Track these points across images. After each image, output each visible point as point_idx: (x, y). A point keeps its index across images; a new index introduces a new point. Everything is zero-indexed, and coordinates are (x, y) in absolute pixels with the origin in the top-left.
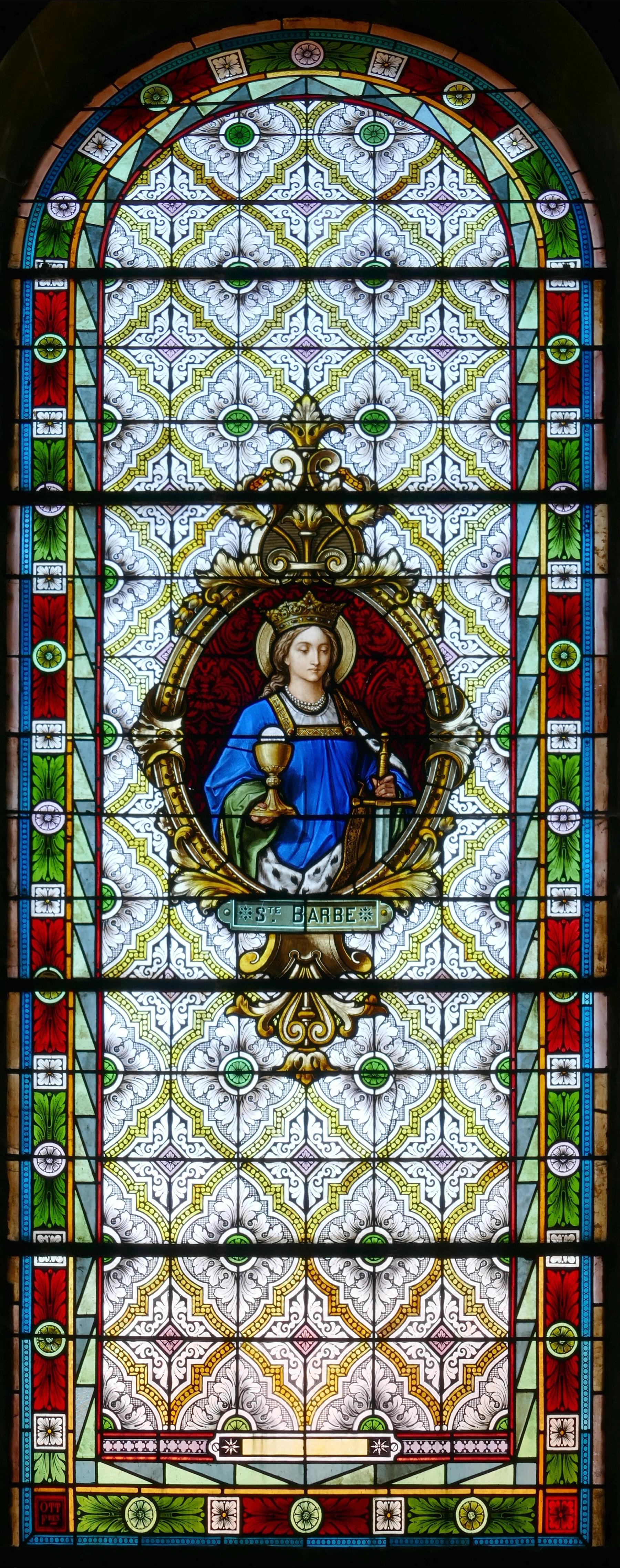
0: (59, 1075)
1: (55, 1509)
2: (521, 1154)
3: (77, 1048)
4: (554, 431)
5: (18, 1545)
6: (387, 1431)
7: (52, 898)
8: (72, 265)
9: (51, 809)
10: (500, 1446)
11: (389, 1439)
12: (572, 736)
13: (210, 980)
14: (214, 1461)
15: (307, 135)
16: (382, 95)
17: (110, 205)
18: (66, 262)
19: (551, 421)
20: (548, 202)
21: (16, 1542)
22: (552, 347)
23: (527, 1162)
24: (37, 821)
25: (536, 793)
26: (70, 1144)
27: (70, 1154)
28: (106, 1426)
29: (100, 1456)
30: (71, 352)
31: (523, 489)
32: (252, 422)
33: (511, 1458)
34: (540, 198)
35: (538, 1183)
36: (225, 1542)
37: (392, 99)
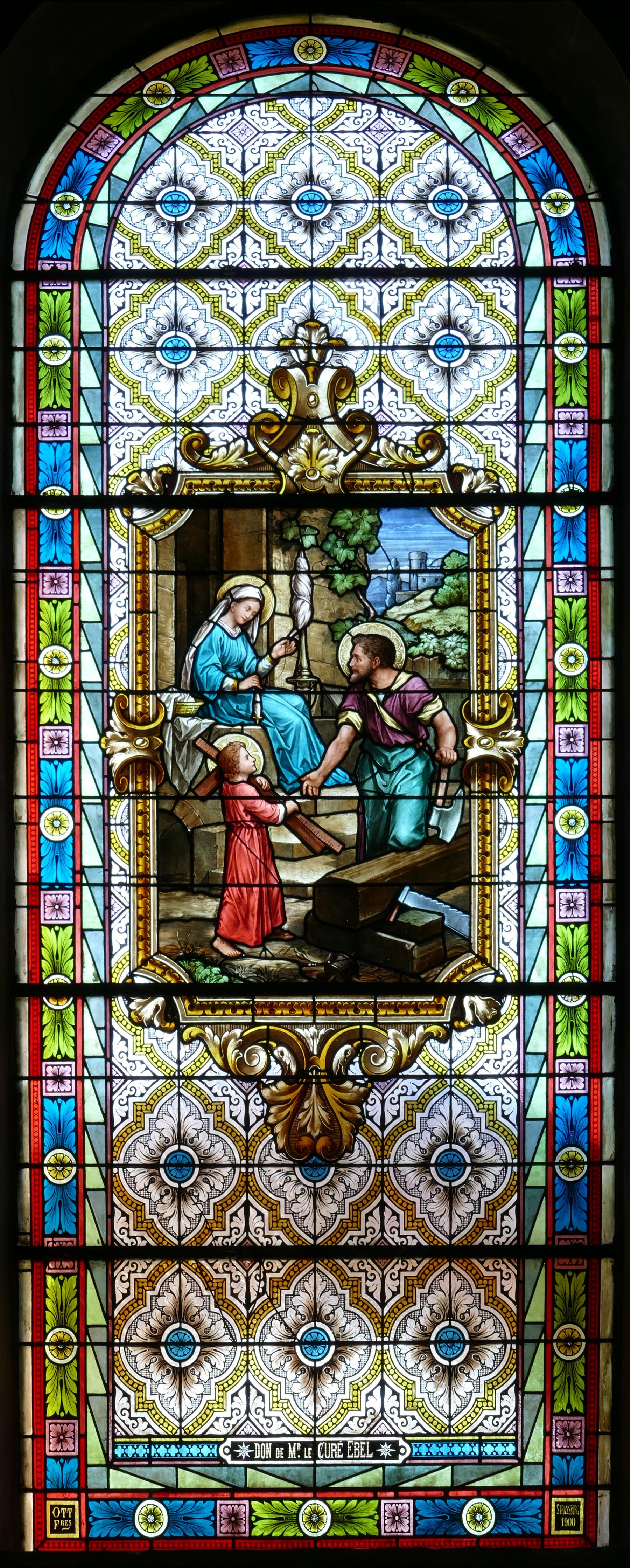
0: (68, 1082)
1: (67, 1515)
2: (528, 1159)
5: (32, 1550)
6: (397, 1435)
11: (397, 1442)
12: (580, 1075)
14: (227, 1465)
15: (311, 132)
16: (388, 94)
17: (112, 206)
21: (30, 1546)
22: (560, 345)
25: (545, 863)
28: (119, 1432)
29: (111, 1463)
34: (544, 198)
36: (237, 1546)
37: (399, 98)
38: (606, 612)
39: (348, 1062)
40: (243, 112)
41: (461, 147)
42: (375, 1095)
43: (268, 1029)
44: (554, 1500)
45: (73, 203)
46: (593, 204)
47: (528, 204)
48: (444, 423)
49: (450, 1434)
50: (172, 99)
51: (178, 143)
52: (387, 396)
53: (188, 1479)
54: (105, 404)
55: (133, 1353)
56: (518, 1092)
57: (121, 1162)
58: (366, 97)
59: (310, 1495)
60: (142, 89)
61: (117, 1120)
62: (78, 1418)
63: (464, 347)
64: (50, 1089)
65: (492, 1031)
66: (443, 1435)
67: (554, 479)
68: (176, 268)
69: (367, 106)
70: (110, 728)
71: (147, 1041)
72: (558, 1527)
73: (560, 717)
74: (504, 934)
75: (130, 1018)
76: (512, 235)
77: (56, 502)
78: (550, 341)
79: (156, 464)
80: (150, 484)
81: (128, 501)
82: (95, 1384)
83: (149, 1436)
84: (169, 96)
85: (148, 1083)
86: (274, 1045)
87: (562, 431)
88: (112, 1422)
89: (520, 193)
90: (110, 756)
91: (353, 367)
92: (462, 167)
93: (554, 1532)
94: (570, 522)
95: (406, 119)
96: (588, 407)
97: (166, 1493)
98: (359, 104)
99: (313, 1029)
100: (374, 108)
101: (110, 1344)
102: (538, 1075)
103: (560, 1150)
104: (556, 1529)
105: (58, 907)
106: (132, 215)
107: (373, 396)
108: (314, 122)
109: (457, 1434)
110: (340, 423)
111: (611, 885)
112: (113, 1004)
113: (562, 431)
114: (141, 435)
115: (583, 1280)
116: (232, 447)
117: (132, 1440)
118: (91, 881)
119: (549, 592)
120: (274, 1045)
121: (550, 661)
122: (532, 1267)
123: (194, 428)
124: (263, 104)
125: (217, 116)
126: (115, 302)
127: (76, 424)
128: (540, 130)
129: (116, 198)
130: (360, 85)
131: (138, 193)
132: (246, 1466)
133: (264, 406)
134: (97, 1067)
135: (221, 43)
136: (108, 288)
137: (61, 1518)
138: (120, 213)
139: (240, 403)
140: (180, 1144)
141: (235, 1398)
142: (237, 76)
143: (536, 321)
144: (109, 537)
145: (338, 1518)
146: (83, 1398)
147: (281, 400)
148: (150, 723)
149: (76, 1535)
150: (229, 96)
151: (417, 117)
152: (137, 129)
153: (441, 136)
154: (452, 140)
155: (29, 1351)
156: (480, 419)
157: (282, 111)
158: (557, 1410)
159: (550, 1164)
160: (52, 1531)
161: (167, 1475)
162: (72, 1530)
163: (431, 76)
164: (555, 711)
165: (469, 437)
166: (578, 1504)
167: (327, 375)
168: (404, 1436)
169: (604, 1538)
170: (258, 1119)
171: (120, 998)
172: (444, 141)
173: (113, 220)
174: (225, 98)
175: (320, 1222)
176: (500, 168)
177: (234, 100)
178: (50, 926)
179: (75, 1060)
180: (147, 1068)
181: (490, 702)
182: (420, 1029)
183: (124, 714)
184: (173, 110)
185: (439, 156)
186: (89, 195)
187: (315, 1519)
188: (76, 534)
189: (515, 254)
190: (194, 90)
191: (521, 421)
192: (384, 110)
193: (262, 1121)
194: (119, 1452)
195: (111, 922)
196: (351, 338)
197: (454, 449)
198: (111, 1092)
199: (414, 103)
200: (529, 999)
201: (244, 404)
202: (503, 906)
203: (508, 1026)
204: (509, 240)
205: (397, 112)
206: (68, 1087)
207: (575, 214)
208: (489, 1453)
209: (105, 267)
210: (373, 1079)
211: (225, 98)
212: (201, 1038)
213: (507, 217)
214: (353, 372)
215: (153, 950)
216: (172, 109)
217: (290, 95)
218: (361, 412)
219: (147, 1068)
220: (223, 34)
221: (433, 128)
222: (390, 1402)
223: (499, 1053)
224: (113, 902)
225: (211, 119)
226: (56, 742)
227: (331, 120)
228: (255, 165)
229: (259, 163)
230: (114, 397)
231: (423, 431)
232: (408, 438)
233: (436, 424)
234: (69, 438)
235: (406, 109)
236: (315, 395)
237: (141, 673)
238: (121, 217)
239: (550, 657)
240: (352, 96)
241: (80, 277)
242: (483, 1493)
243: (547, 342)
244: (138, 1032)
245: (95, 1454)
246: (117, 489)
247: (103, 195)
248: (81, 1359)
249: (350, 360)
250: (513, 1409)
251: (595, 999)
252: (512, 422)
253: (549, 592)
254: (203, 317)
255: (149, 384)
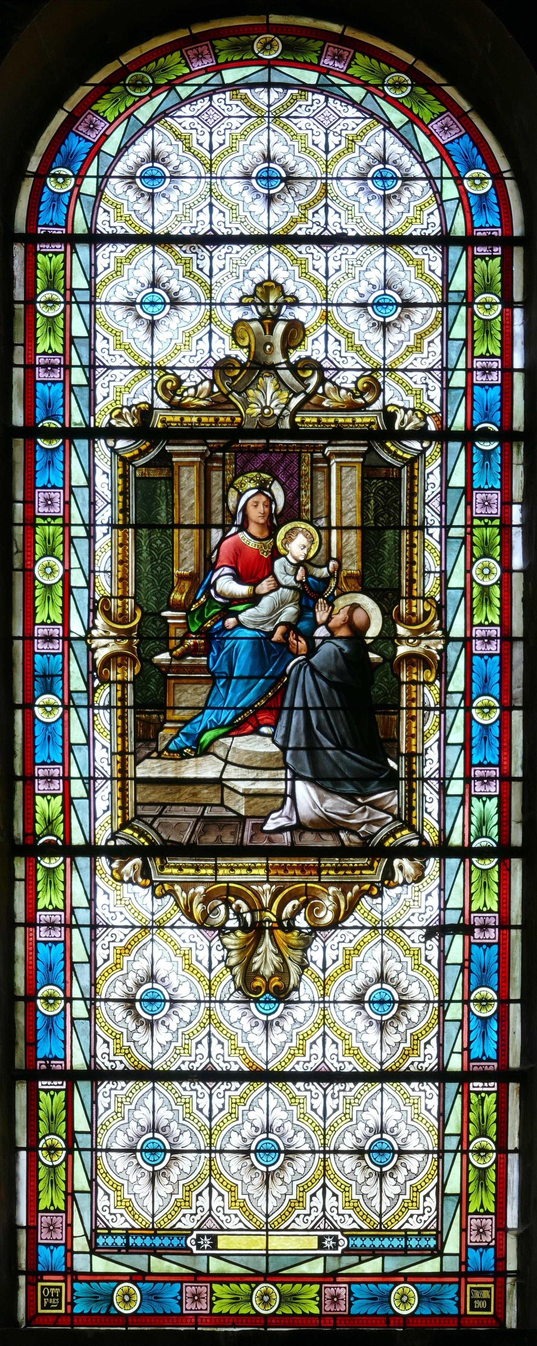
1: (55, 1294)
3: (74, 905)
4: (479, 378)
6: (336, 1229)
7: (52, 778)
8: (69, 231)
9: (52, 702)
10: (430, 1243)
13: (358, 1073)
14: (192, 1254)
16: (334, 85)
18: (64, 230)
19: (476, 638)
20: (473, 179)
23: (452, 1004)
24: (38, 711)
26: (68, 985)
27: (68, 995)
30: (68, 306)
31: (453, 429)
32: (164, 177)
33: (438, 1252)
34: (467, 176)
35: (461, 1021)
38: (513, 1171)
39: (296, 912)
40: (211, 100)
41: (397, 133)
42: (317, 943)
43: (228, 886)
44: (469, 1286)
45: (65, 177)
46: (507, 181)
47: (452, 181)
48: (380, 369)
49: (381, 1230)
50: (150, 88)
51: (156, 125)
52: (332, 346)
53: (158, 1265)
54: (92, 350)
55: (113, 1008)
56: (440, 516)
57: (103, 997)
58: (316, 88)
59: (262, 1279)
60: (125, 81)
61: (100, 961)
62: (66, 1212)
63: (397, 178)
64: (41, 787)
65: (417, 889)
66: (375, 1230)
67: (469, 984)
68: (153, 233)
69: (316, 96)
70: (95, 627)
71: (126, 895)
72: (472, 1309)
73: (476, 621)
74: (427, 805)
75: (112, 876)
76: (438, 208)
77: (50, 434)
78: (470, 300)
79: (136, 402)
80: (129, 422)
81: (111, 433)
82: (81, 1182)
83: (127, 1229)
84: (148, 85)
85: (126, 931)
86: (232, 899)
87: (479, 378)
88: (95, 1216)
89: (446, 173)
90: (94, 651)
91: (302, 319)
92: (396, 149)
93: (469, 1312)
94: (487, 454)
95: (350, 107)
96: (501, 357)
97: (138, 1277)
98: (310, 94)
99: (267, 886)
100: (322, 98)
101: (92, 302)
102: (458, 708)
103: (474, 990)
104: (471, 1310)
105: (51, 1228)
106: (115, 187)
107: (320, 345)
108: (271, 109)
109: (386, 1230)
110: (293, 368)
111: (520, 529)
112: (97, 864)
113: (478, 378)
114: (123, 377)
115: (494, 1100)
116: (200, 387)
117: (110, 1232)
118: (81, 1146)
119: (469, 513)
120: (232, 899)
121: (468, 571)
122: (455, 252)
123: (168, 371)
124: (228, 94)
125: (190, 103)
126: (101, 263)
127: (68, 367)
128: (461, 116)
129: (102, 173)
130: (311, 77)
131: (120, 169)
132: (208, 1255)
133: (228, 352)
134: (83, 917)
135: (194, 39)
136: (96, 250)
137: (49, 1297)
138: (106, 186)
139: (207, 350)
140: (153, 1133)
141: (200, 1198)
142: (205, 69)
143: (459, 282)
144: (96, 1033)
145: (285, 1299)
146: (70, 1195)
147: (242, 347)
148: (129, 623)
149: (63, 1311)
150: (200, 86)
151: (358, 106)
152: (120, 114)
153: (379, 122)
154: (389, 126)
155: (23, 1155)
156: (410, 367)
157: (245, 99)
158: (471, 1210)
159: (465, 1002)
160: (43, 1308)
161: (140, 1261)
162: (59, 1307)
163: (372, 71)
164: (472, 616)
165: (400, 382)
166: (489, 1289)
167: (280, 328)
168: (342, 1230)
169: (511, 1320)
170: (220, 962)
171: (103, 858)
172: (382, 127)
173: (100, 190)
174: (196, 87)
175: (272, 1049)
176: (430, 152)
177: (205, 89)
178: (44, 796)
179: (63, 488)
180: (126, 918)
181: (416, 691)
182: (356, 887)
183: (108, 614)
184: (152, 98)
185: (377, 264)
186: (79, 171)
187: (265, 1299)
188: (66, 462)
189: (441, 225)
190: (170, 81)
191: (446, 370)
192: (331, 100)
193: (223, 964)
194: (100, 1241)
195: (95, 380)
196: (302, 295)
197: (388, 393)
198: (94, 940)
199: (357, 93)
200: (448, 861)
201: (210, 350)
202: (427, 504)
203: (431, 883)
204: (436, 213)
205: (341, 101)
206: (58, 934)
207: (493, 191)
208: (414, 1246)
209: (93, 1067)
210: (315, 929)
211: (196, 87)
212: (172, 893)
213: (434, 193)
214: (303, 324)
215: (131, 816)
216: (151, 96)
217: (252, 86)
218: (308, 358)
219: (126, 918)
220: (194, 31)
221: (372, 115)
222: (331, 1202)
223: (423, 907)
224: (97, 499)
225: (184, 106)
226: (51, 1228)
227: (285, 107)
228: (221, 145)
229: (224, 143)
230: (100, 344)
231: (362, 376)
232: (350, 381)
233: (374, 370)
234: (63, 1241)
235: (351, 99)
236: (271, 345)
237: (121, 545)
238: (106, 190)
239: (468, 568)
240: (303, 87)
241: (71, 240)
242: (409, 1279)
243: (468, 299)
244: (118, 888)
245: (80, 1244)
246: (102, 421)
247: (92, 171)
248: (68, 1160)
249: (300, 314)
250: (434, 1208)
251: (507, 444)
252: (435, 779)
253: (469, 513)
254: (176, 276)
255: (131, 205)
